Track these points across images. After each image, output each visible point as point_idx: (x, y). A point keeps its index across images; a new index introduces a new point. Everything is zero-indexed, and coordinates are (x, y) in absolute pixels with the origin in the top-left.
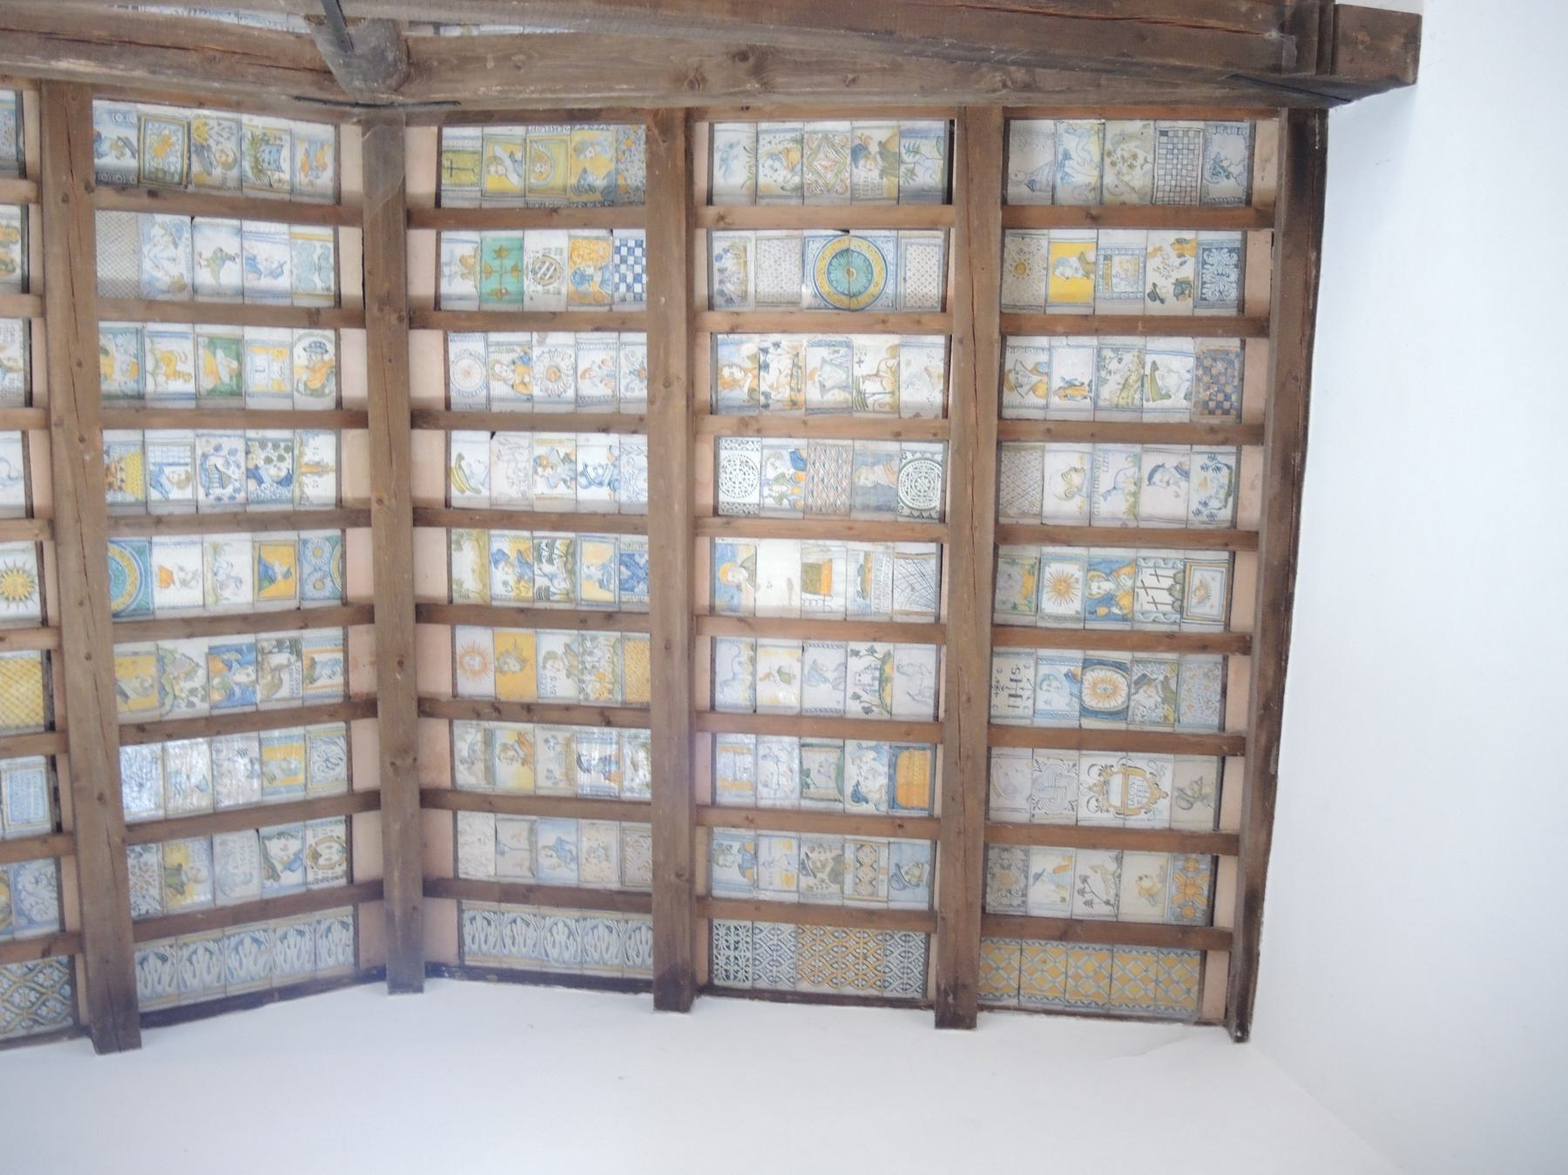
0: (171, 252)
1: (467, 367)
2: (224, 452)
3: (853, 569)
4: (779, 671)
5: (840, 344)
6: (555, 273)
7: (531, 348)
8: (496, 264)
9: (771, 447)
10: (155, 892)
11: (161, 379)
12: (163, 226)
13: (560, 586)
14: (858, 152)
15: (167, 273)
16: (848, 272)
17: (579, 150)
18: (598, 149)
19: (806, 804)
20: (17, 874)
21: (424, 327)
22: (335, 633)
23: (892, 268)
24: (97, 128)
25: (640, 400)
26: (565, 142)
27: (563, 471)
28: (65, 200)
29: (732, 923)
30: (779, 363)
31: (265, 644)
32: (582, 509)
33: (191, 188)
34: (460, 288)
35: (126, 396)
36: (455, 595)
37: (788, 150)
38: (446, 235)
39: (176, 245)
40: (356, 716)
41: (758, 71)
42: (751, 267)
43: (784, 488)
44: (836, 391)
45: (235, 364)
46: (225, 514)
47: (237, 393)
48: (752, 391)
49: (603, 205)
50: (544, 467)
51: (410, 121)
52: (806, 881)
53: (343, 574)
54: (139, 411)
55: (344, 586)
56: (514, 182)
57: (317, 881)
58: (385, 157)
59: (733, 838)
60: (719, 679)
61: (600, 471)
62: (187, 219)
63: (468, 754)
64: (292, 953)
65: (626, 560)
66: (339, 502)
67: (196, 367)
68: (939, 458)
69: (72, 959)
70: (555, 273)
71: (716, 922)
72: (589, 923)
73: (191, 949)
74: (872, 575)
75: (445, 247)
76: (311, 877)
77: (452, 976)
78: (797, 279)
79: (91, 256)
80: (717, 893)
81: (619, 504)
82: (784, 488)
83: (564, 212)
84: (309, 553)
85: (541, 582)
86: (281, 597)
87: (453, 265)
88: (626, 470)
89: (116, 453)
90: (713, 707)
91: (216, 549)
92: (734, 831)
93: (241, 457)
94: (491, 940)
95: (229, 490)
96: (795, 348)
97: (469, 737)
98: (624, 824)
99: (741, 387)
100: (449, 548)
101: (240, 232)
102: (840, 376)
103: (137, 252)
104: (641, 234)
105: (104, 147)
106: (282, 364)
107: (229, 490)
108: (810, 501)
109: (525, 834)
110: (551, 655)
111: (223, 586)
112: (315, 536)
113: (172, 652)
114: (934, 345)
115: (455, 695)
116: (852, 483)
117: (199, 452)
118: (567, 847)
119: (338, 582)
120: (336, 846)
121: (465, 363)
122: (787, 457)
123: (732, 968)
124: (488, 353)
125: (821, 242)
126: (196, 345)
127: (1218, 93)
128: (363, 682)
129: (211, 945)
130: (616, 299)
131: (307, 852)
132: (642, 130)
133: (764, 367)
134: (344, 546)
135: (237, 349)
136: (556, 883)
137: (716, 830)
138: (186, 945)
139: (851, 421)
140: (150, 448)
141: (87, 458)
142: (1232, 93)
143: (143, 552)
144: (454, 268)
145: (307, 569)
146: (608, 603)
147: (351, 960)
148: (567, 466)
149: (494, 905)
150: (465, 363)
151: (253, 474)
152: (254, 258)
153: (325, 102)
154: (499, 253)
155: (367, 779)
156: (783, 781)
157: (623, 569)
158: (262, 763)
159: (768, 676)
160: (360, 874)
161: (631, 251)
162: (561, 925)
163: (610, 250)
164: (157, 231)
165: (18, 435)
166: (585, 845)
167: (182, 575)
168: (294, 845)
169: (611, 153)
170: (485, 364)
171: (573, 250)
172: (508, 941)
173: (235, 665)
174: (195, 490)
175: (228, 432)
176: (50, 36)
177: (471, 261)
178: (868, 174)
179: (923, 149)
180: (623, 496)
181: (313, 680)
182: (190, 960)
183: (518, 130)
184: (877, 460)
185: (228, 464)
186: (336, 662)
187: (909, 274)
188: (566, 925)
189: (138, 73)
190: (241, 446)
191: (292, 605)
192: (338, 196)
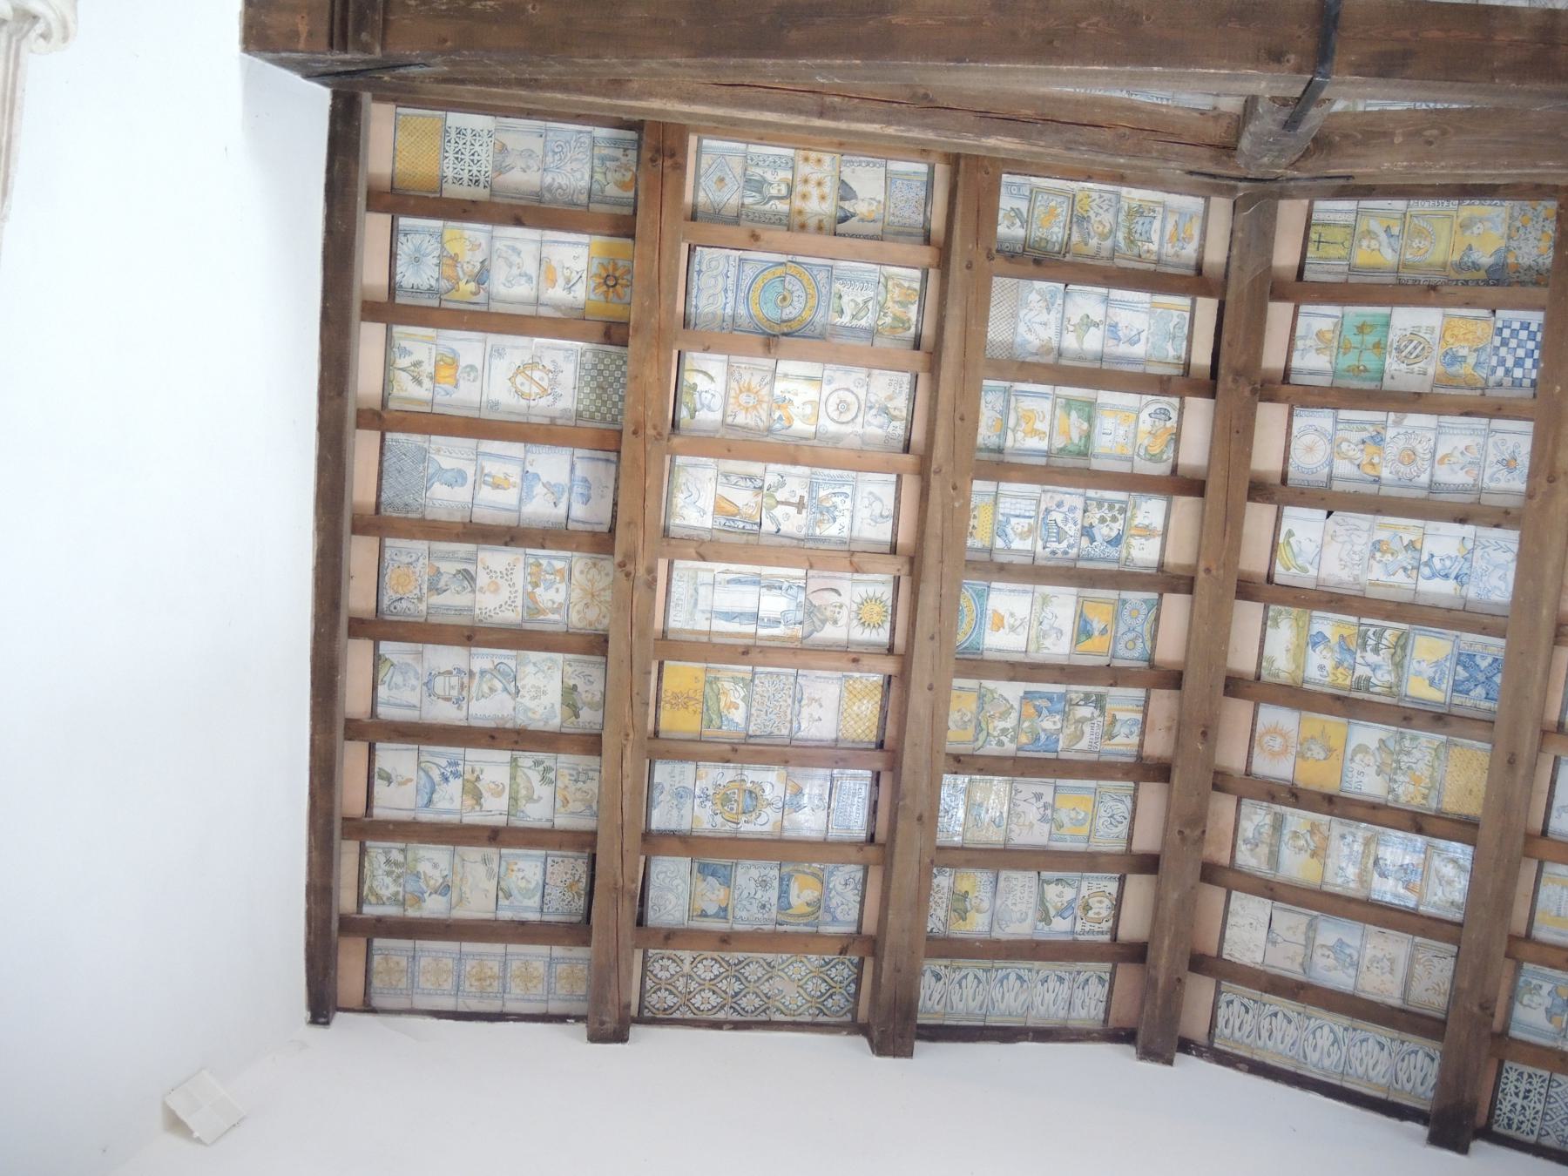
0: (1044, 317)
1: (1311, 443)
2: (1065, 509)
7: (1385, 428)
8: (1355, 340)
11: (1020, 435)
12: (1039, 292)
13: (1383, 677)
15: (1038, 337)
17: (1464, 226)
18: (1488, 225)
20: (831, 874)
21: (1271, 400)
22: (1139, 693)
25: (1518, 493)
26: (1449, 216)
27: (1404, 558)
28: (969, 267)
29: (1528, 1069)
31: (1073, 696)
33: (1068, 258)
34: (1312, 362)
36: (1264, 673)
38: (1303, 308)
40: (1147, 779)
45: (1085, 426)
46: (1057, 568)
47: (1084, 454)
49: (1487, 283)
51: (1283, 195)
54: (1000, 467)
55: (1153, 648)
56: (1388, 257)
57: (1083, 933)
58: (1255, 230)
59: (1546, 978)
60: (1556, 804)
61: (1448, 563)
62: (1062, 286)
63: (1251, 834)
64: (1050, 997)
65: (1465, 660)
66: (1161, 566)
69: (862, 960)
70: (1424, 351)
71: (1507, 1064)
72: (1360, 1035)
73: (963, 973)
75: (1301, 321)
76: (1078, 928)
77: (1200, 1055)
79: (984, 320)
80: (1515, 1033)
81: (1466, 601)
83: (1445, 289)
84: (1125, 613)
85: (1362, 671)
86: (1094, 653)
87: (1310, 339)
88: (1479, 564)
89: (975, 500)
90: (1544, 832)
91: (1046, 600)
92: (1547, 971)
93: (1079, 514)
94: (1247, 1028)
95: (1064, 545)
97: (1256, 818)
98: (1418, 939)
100: (1265, 624)
101: (1106, 300)
103: (1015, 316)
104: (1536, 318)
106: (1128, 428)
107: (1064, 545)
109: (1303, 928)
110: (1362, 749)
111: (1045, 635)
112: (1135, 597)
113: (992, 692)
115: (1248, 773)
117: (1043, 507)
118: (1348, 951)
119: (1148, 644)
120: (1107, 902)
123: (1516, 1118)
126: (1054, 406)
127: (1452, 100)
128: (1158, 745)
129: (980, 973)
130: (1491, 383)
131: (1080, 902)
134: (1159, 610)
135: (1089, 412)
136: (1329, 985)
137: (1526, 966)
138: (959, 968)
142: (1482, 102)
143: (982, 596)
144: (1309, 342)
145: (1122, 628)
146: (1437, 704)
147: (1102, 1016)
149: (1257, 994)
150: (1308, 439)
151: (1087, 532)
152: (1115, 326)
153: (1214, 176)
154: (1361, 329)
155: (1146, 842)
157: (1459, 669)
158: (1054, 810)
160: (1125, 934)
161: (1515, 333)
162: (1326, 1029)
164: (1034, 297)
165: (893, 477)
166: (1369, 952)
167: (1012, 621)
168: (1069, 893)
169: (1503, 229)
170: (1331, 441)
172: (1265, 1034)
173: (1045, 712)
174: (1035, 542)
176: (984, 115)
181: (1112, 737)
182: (960, 983)
183: (1399, 205)
185: (1066, 520)
188: (1332, 1031)
189: (1055, 151)
190: (1078, 502)
191: (1103, 661)
192: (1199, 268)
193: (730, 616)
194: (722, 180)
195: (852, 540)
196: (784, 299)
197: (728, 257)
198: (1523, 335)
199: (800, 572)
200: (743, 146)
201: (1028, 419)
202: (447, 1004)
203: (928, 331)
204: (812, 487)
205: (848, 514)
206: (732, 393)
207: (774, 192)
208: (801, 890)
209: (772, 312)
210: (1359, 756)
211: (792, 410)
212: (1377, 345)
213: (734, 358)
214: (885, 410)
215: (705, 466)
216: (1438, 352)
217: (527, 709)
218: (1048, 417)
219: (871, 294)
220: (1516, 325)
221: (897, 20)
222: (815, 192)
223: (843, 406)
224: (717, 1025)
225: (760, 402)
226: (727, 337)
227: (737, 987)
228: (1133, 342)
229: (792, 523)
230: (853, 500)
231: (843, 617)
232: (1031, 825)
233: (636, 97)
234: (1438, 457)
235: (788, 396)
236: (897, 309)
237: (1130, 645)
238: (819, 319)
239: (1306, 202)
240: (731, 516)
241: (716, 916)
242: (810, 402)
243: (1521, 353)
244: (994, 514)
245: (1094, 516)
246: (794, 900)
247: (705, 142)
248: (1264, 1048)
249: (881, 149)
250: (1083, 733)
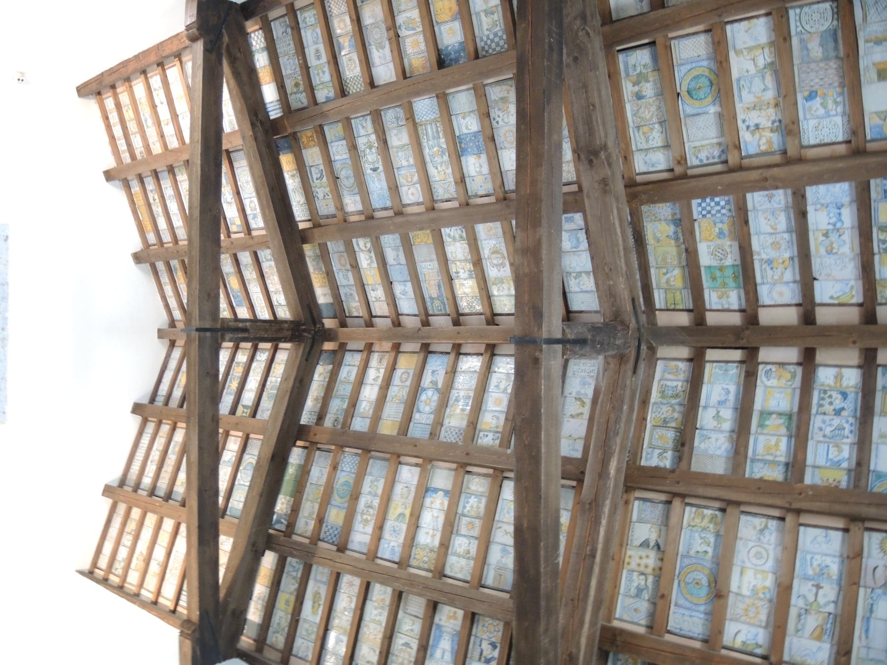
0: (713, 440)
1: (778, 296)
2: (823, 426)
3: (878, 49)
5: (738, 84)
6: (721, 248)
8: (719, 281)
9: (805, 114)
11: (778, 453)
14: (639, 96)
16: (699, 88)
17: (658, 241)
23: (694, 65)
24: (653, 465)
27: (834, 237)
30: (754, 118)
32: (856, 224)
35: (786, 471)
37: (644, 133)
38: (708, 307)
39: (710, 438)
41: (596, 153)
42: (704, 142)
43: (830, 102)
44: (766, 82)
45: (774, 416)
47: (790, 416)
48: (772, 131)
50: (832, 248)
54: (796, 465)
56: (677, 272)
61: (831, 215)
67: (773, 435)
68: (798, 11)
74: (880, 35)
75: (714, 307)
78: (706, 117)
81: (851, 202)
82: (830, 102)
88: (828, 199)
89: (818, 482)
93: (827, 418)
95: (847, 426)
96: (744, 111)
99: (771, 138)
101: (705, 407)
102: (757, 81)
103: (712, 456)
105: (662, 465)
106: (776, 391)
108: (836, 84)
114: (732, 31)
117: (821, 439)
121: (775, 295)
122: (810, 103)
124: (767, 283)
125: (686, 107)
132: (644, 208)
133: (757, 126)
135: (765, 414)
139: (783, 67)
140: (817, 464)
141: (810, 493)
144: (724, 302)
148: (830, 234)
150: (775, 295)
151: (838, 412)
154: (714, 279)
161: (704, 209)
163: (704, 220)
164: (702, 446)
165: (802, 529)
169: (657, 224)
170: (774, 284)
171: (707, 240)
174: (844, 443)
175: (812, 423)
178: (649, 89)
179: (633, 63)
180: (846, 200)
183: (653, 271)
184: (805, 47)
185: (830, 425)
187: (696, 54)
190: (819, 418)
192: (690, 360)
194: (636, 610)
195: (841, 556)
196: (697, 583)
197: (674, 613)
198: (704, 205)
199: (862, 591)
200: (620, 597)
201: (769, 448)
203: (717, 504)
204: (807, 578)
205: (824, 558)
206: (748, 620)
207: (643, 583)
209: (704, 592)
211: (759, 586)
213: (728, 616)
214: (762, 531)
215: (791, 644)
216: (719, 242)
218: (768, 437)
219: (697, 535)
220: (700, 209)
221: (525, 525)
222: (644, 561)
223: (758, 556)
225: (753, 604)
226: (716, 620)
228: (728, 392)
229: (829, 593)
230: (816, 554)
233: (579, 650)
234: (772, 231)
235: (751, 588)
236: (706, 520)
238: (708, 565)
239: (657, 312)
240: (823, 631)
242: (755, 574)
243: (713, 204)
244: (826, 468)
245: (828, 408)
247: (617, 616)
249: (626, 523)
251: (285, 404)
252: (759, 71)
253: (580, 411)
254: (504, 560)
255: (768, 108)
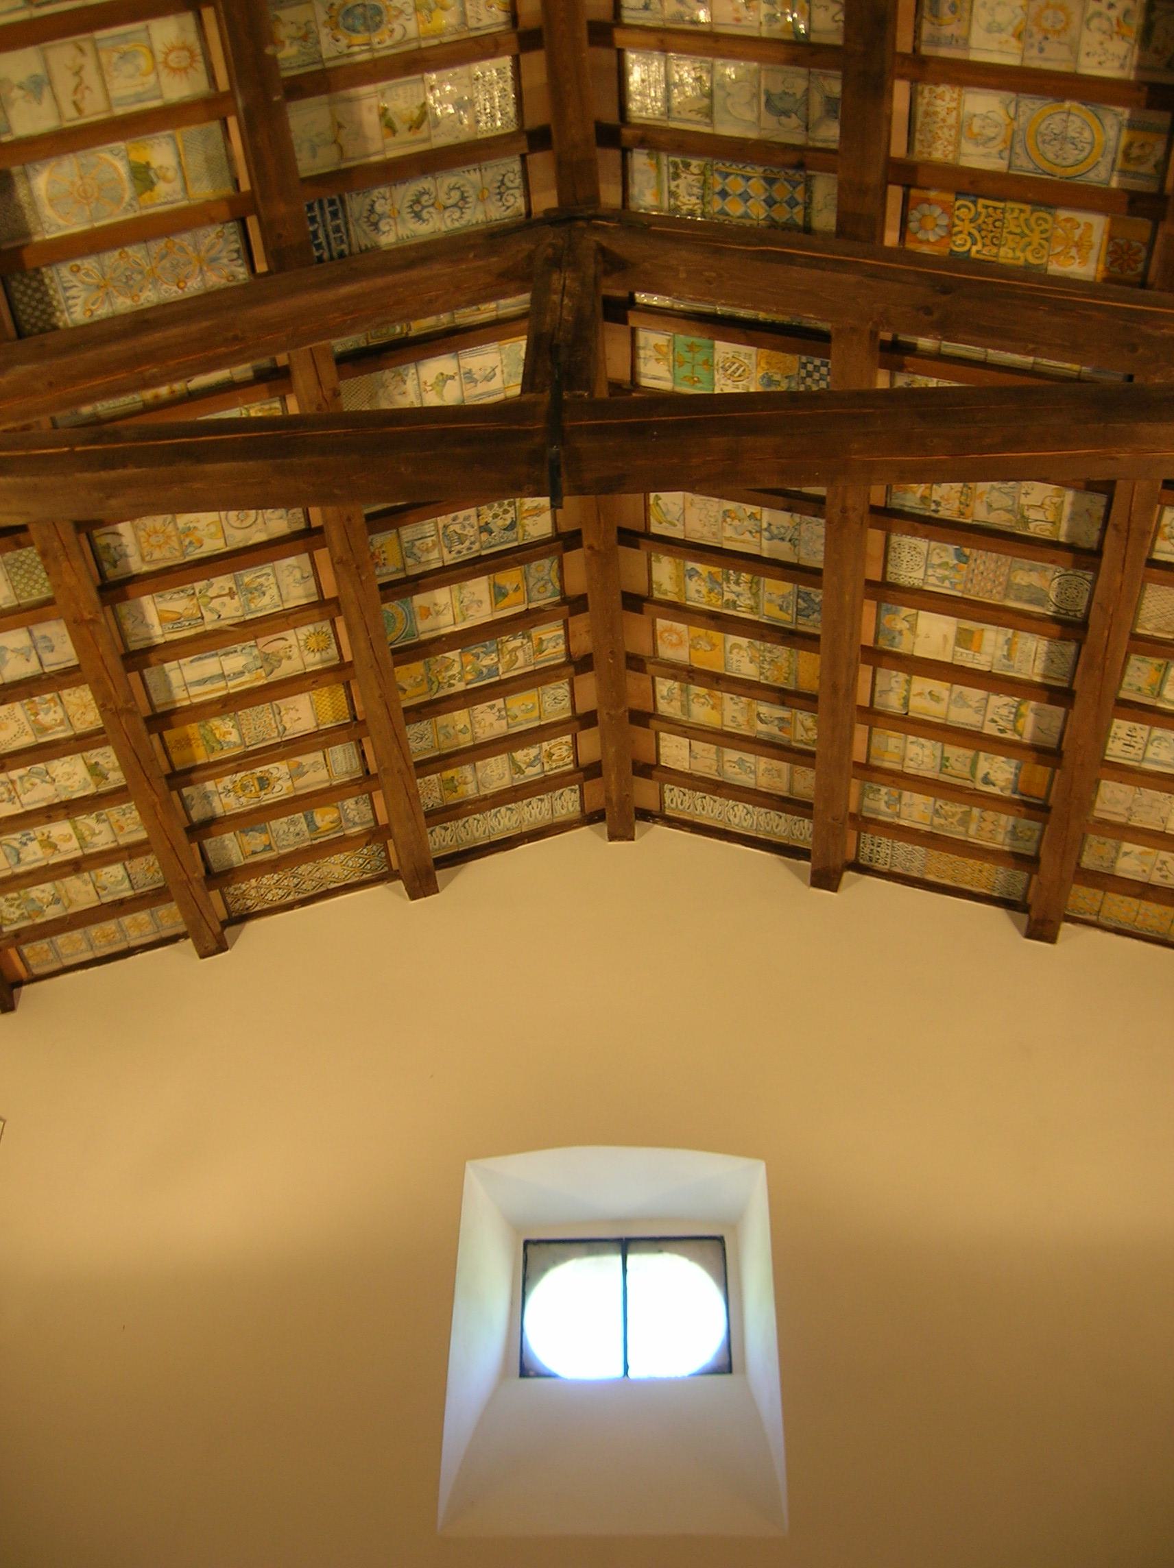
2: (461, 520)
4: (930, 693)
10: (437, 794)
19: (943, 778)
43: (947, 573)
52: (937, 821)
53: (561, 579)
60: (878, 689)
61: (782, 530)
82: (947, 573)
94: (686, 804)
95: (467, 543)
107: (467, 543)
116: (1008, 580)
119: (557, 584)
131: (543, 754)
144: (649, 353)
145: (532, 581)
147: (579, 808)
148: (752, 522)
152: (470, 372)
156: (926, 760)
159: (920, 694)
172: (699, 808)
173: (482, 655)
174: (441, 552)
177: (665, 349)
182: (464, 826)
185: (464, 527)
186: (559, 636)
193: (203, 682)
202: (88, 956)
205: (274, 587)
206: (143, 540)
208: (323, 817)
210: (735, 651)
211: (199, 534)
212: (706, 363)
217: (66, 788)
224: (289, 907)
225: (169, 537)
227: (296, 881)
230: (275, 576)
231: (295, 652)
232: (491, 725)
237: (542, 590)
241: (264, 850)
244: (400, 545)
246: (319, 824)
248: (700, 815)
250: (517, 658)
251: (327, 170)
252: (1021, 507)
253: (398, 125)
254: (17, 93)
255: (961, 503)
